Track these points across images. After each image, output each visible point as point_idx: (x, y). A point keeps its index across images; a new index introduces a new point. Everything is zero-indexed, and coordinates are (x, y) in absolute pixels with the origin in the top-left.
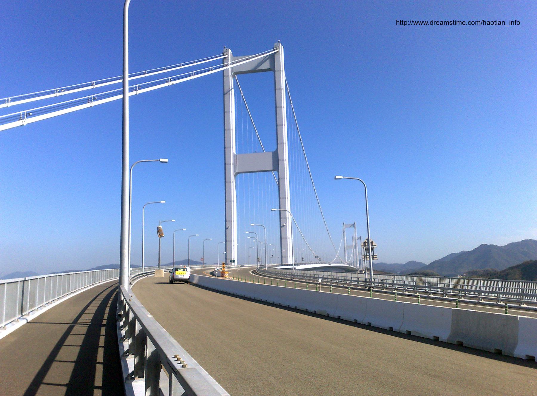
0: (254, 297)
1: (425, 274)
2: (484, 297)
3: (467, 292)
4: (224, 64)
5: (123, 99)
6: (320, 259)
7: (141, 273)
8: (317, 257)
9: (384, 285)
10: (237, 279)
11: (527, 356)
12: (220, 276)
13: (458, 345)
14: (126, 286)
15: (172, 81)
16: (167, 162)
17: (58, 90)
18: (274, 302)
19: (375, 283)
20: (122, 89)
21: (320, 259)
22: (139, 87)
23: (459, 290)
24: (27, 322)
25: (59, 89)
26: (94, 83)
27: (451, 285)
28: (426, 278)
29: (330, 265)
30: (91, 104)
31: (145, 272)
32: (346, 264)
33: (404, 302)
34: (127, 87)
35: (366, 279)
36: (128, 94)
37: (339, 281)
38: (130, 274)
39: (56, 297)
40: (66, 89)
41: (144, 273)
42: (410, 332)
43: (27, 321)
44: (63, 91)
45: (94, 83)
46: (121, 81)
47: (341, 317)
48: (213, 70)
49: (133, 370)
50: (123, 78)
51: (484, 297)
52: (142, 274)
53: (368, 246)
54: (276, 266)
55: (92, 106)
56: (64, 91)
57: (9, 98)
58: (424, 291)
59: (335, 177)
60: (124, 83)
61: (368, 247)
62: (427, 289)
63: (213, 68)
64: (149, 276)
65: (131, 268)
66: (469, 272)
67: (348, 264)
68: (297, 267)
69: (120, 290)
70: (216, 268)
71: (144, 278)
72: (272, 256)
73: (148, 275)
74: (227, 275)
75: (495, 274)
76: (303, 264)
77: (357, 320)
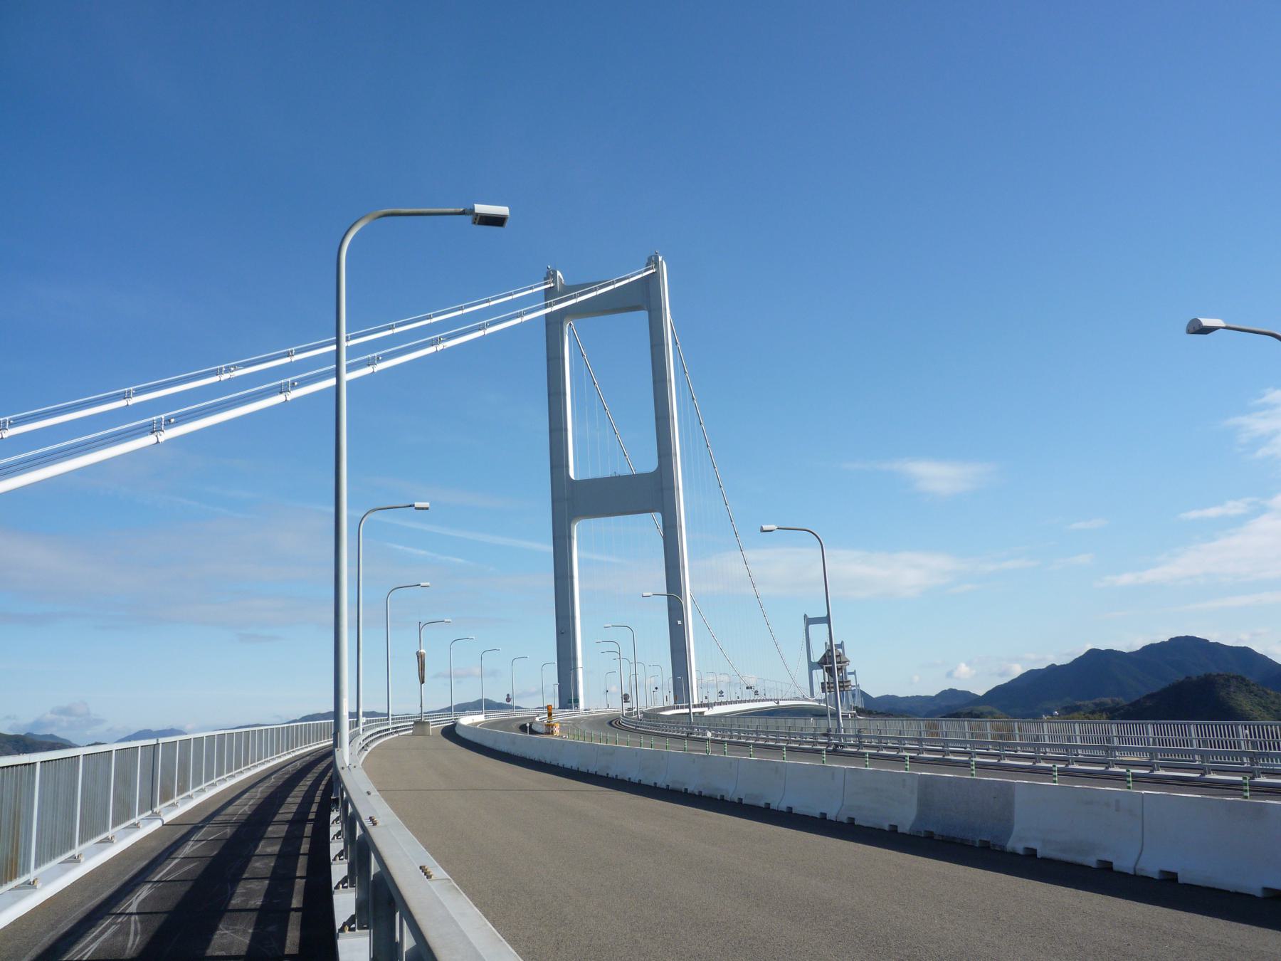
0: (595, 770)
1: (976, 714)
2: (1083, 757)
3: (1019, 748)
4: (544, 303)
5: (338, 386)
6: (756, 693)
7: (386, 727)
8: (751, 688)
9: (863, 740)
10: (572, 737)
11: (1162, 872)
12: (541, 731)
13: (927, 838)
14: (345, 756)
15: (443, 341)
16: (427, 509)
17: (224, 369)
18: (655, 784)
19: (845, 737)
20: (334, 366)
21: (756, 693)
22: (378, 358)
23: (1067, 747)
24: (163, 825)
25: (225, 367)
26: (292, 351)
27: (1046, 736)
28: (943, 722)
29: (778, 703)
30: (159, 436)
31: (395, 726)
32: (813, 701)
33: (919, 773)
34: (344, 363)
35: (829, 730)
36: (347, 377)
37: (790, 737)
38: (363, 730)
39: (213, 779)
40: (239, 365)
41: (393, 728)
42: (896, 826)
43: (163, 822)
44: (232, 369)
45: (292, 351)
46: (334, 347)
47: (771, 805)
48: (526, 314)
49: (354, 913)
50: (338, 342)
51: (1083, 757)
52: (388, 730)
53: (830, 663)
54: (664, 709)
55: (289, 399)
56: (235, 370)
57: (131, 388)
58: (1013, 753)
59: (762, 527)
60: (338, 351)
61: (831, 662)
62: (968, 745)
63: (487, 323)
64: (401, 734)
65: (365, 718)
66: (1066, 708)
67: (817, 700)
68: (708, 712)
69: (333, 765)
70: (538, 716)
71: (393, 738)
72: (656, 688)
73: (401, 731)
74: (557, 730)
75: (1118, 710)
76: (720, 704)
77: (825, 814)
